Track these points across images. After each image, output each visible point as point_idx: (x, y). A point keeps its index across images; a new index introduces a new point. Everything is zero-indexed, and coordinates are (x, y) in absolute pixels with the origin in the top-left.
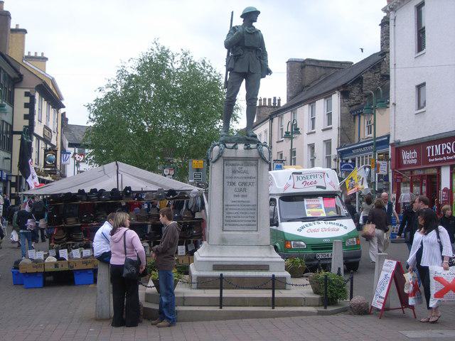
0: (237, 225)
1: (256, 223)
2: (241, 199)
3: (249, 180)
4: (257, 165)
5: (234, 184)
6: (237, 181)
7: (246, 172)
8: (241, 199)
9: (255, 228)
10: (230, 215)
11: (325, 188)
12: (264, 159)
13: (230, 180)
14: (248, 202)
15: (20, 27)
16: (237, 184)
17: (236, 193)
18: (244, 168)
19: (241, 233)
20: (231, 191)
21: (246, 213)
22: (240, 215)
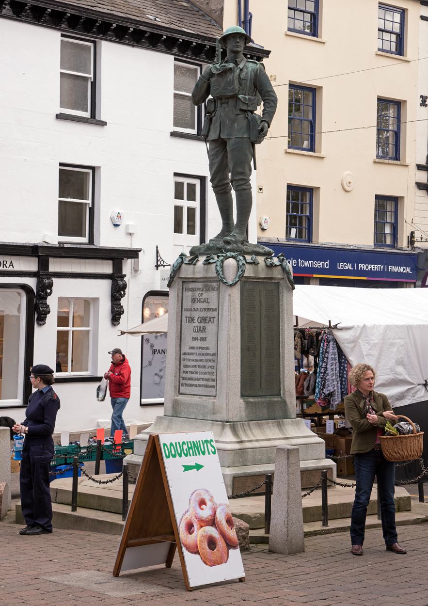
2: (198, 344)
4: (218, 290)
5: (193, 320)
7: (206, 301)
9: (212, 391)
11: (263, 47)
14: (207, 348)
16: (196, 321)
17: (195, 335)
19: (196, 398)
20: (189, 330)
21: (204, 367)
22: (198, 370)
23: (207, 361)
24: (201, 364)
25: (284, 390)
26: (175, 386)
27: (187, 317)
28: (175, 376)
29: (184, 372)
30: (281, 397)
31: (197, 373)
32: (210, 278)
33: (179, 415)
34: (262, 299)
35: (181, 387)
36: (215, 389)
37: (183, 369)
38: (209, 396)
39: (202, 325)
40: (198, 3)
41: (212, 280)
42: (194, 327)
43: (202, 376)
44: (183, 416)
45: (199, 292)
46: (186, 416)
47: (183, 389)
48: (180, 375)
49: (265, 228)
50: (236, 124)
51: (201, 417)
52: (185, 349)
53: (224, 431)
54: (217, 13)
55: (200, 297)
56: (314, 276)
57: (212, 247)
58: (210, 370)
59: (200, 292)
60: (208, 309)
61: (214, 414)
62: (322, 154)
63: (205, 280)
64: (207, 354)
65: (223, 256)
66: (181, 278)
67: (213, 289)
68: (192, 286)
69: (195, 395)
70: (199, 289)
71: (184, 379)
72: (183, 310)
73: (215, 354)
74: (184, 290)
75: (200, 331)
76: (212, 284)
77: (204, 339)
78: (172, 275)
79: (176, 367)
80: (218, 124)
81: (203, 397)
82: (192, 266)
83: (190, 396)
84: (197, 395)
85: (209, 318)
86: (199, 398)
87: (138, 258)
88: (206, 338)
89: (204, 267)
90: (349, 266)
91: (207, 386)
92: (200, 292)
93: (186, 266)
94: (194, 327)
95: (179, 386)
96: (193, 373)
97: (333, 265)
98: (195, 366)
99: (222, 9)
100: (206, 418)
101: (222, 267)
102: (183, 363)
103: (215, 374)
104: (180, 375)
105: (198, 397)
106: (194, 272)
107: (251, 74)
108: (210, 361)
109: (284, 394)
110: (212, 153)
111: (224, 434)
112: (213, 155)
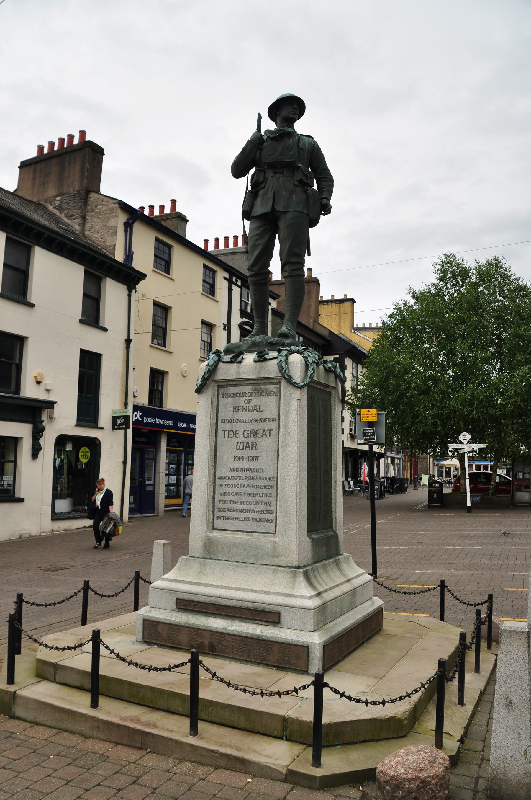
0: (237, 518)
1: (272, 516)
2: (245, 465)
3: (262, 426)
4: (278, 393)
5: (235, 434)
6: (241, 428)
7: (258, 409)
8: (245, 465)
9: (270, 527)
10: (227, 498)
12: (290, 381)
13: (228, 426)
14: (260, 471)
15: (348, 297)
16: (240, 433)
17: (239, 453)
18: (255, 401)
21: (255, 495)
22: (244, 498)
23: (259, 487)
24: (250, 491)
25: (336, 521)
26: (207, 520)
27: (225, 431)
28: (208, 507)
29: (220, 501)
30: (333, 531)
31: (242, 502)
32: (265, 379)
33: (214, 557)
34: (321, 410)
35: (215, 520)
36: (273, 524)
37: (218, 497)
38: (263, 533)
39: (251, 440)
40: (97, 242)
41: (267, 381)
42: (238, 443)
43: (251, 507)
44: (220, 558)
45: (245, 398)
46: (226, 559)
47: (218, 523)
48: (214, 505)
49: (136, 395)
50: (294, 196)
51: (252, 561)
52: (222, 471)
53: (297, 582)
54: (111, 248)
55: (248, 405)
56: (165, 430)
57: (259, 342)
58: (265, 499)
59: (248, 398)
60: (261, 420)
61: (274, 557)
62: (171, 350)
63: (257, 382)
64: (260, 478)
65: (286, 350)
66: (217, 381)
67: (269, 393)
68: (232, 390)
69: (240, 531)
70: (245, 394)
71: (220, 510)
72: (219, 421)
73: (273, 478)
74: (221, 396)
75: (248, 449)
76: (267, 386)
77: (255, 459)
78: (206, 376)
79: (209, 495)
80: (270, 195)
81: (254, 534)
82: (235, 365)
83: (232, 532)
84: (243, 532)
85: (262, 431)
86: (247, 535)
87: (53, 408)
88: (257, 457)
89: (255, 366)
90: (184, 425)
91: (260, 520)
92: (248, 398)
93: (226, 365)
94: (238, 443)
95: (213, 519)
96: (237, 502)
97: (176, 424)
98: (240, 494)
99: (115, 245)
100: (260, 562)
101: (287, 363)
102: (218, 490)
103: (274, 503)
104: (214, 505)
105: (245, 533)
106: (239, 373)
107: (308, 146)
108: (265, 487)
109: (336, 526)
110: (256, 233)
111: (297, 585)
112: (257, 235)
